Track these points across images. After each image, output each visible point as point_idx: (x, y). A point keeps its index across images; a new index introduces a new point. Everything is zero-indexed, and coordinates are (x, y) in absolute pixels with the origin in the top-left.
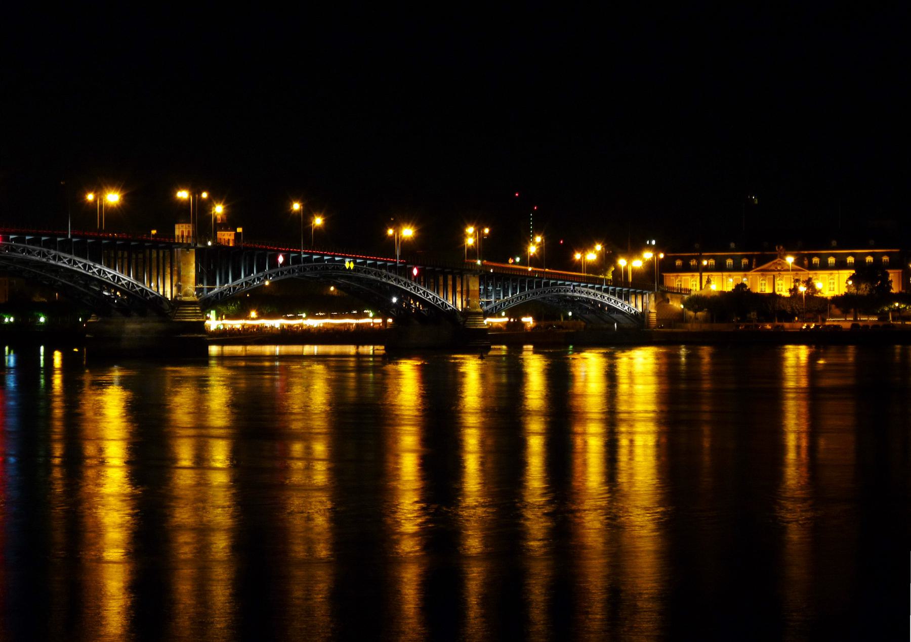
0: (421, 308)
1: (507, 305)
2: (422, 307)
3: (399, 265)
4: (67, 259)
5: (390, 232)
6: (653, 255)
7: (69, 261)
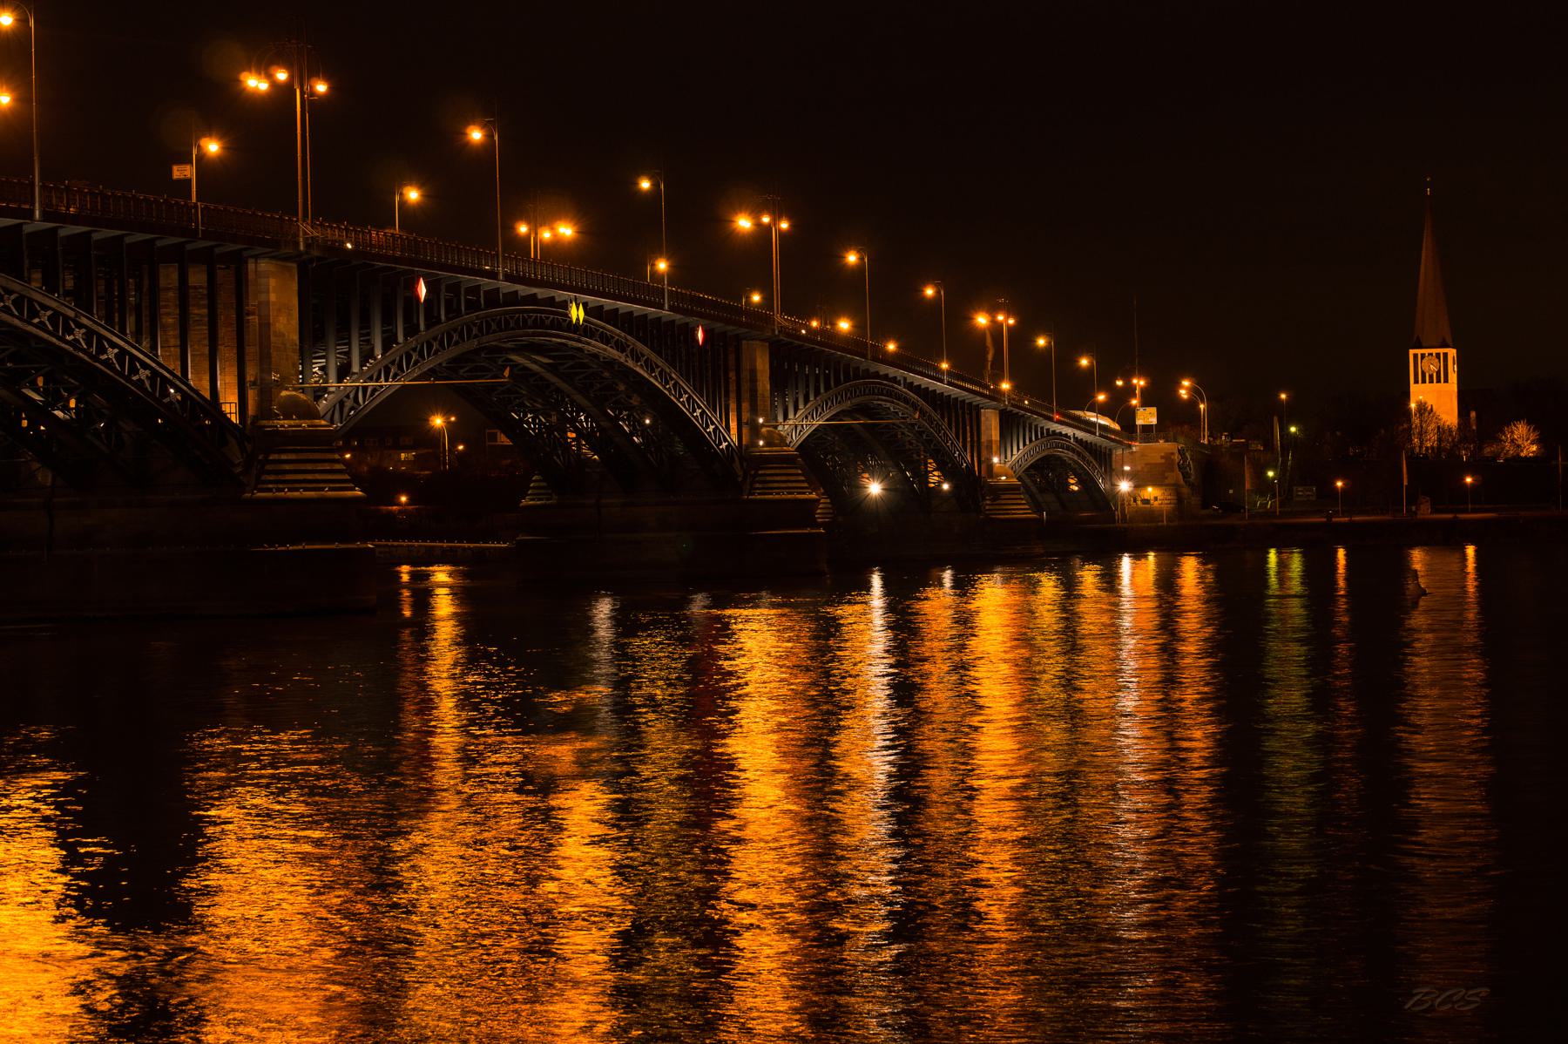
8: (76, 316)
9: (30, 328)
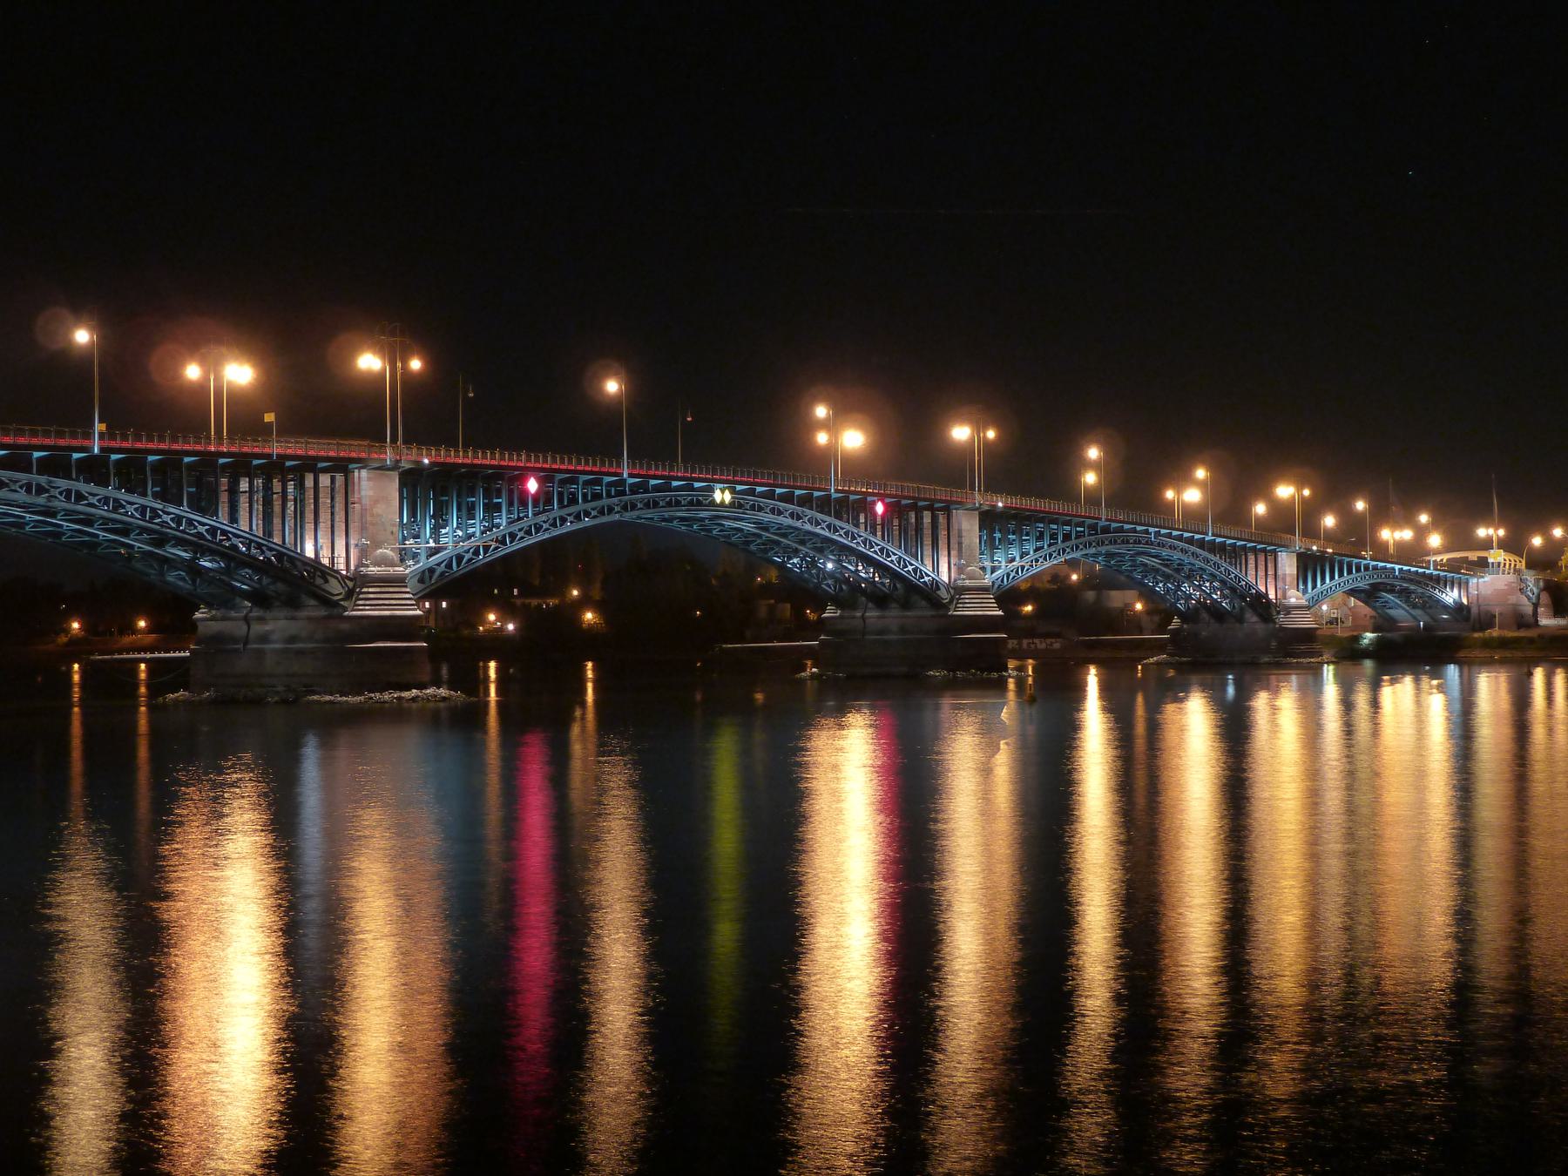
0: (877, 579)
1: (1028, 570)
2: (880, 577)
3: (834, 496)
4: (58, 490)
5: (991, 434)
6: (973, 433)
7: (829, 527)
8: (164, 507)
9: (869, 553)
